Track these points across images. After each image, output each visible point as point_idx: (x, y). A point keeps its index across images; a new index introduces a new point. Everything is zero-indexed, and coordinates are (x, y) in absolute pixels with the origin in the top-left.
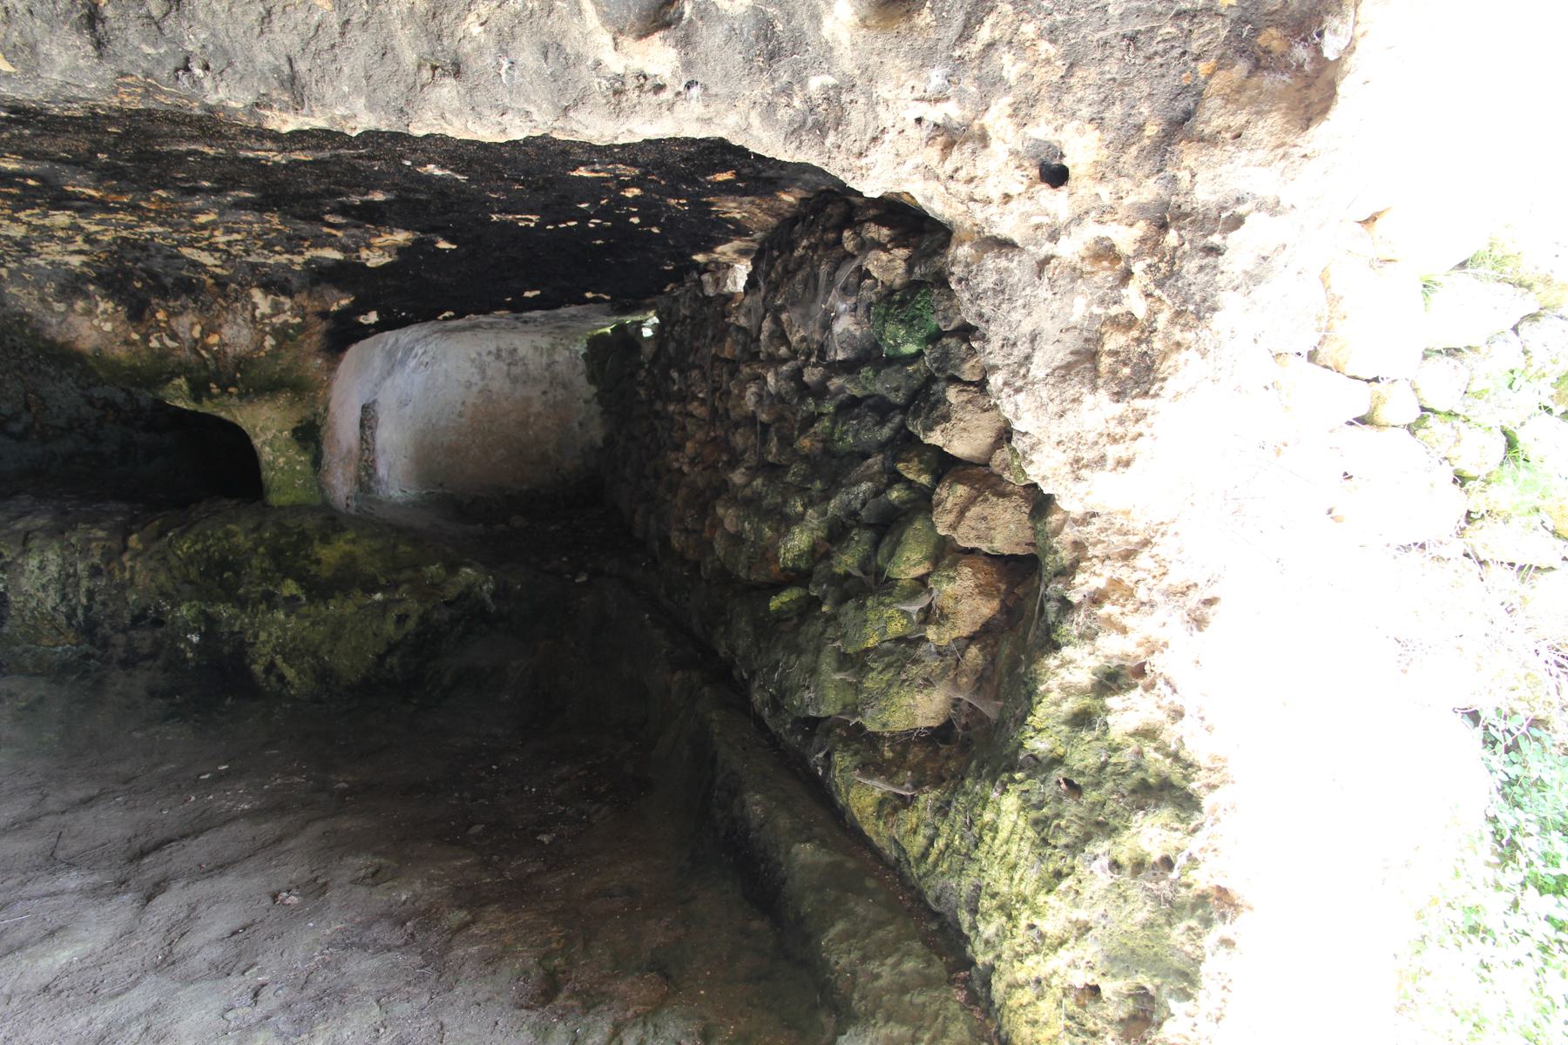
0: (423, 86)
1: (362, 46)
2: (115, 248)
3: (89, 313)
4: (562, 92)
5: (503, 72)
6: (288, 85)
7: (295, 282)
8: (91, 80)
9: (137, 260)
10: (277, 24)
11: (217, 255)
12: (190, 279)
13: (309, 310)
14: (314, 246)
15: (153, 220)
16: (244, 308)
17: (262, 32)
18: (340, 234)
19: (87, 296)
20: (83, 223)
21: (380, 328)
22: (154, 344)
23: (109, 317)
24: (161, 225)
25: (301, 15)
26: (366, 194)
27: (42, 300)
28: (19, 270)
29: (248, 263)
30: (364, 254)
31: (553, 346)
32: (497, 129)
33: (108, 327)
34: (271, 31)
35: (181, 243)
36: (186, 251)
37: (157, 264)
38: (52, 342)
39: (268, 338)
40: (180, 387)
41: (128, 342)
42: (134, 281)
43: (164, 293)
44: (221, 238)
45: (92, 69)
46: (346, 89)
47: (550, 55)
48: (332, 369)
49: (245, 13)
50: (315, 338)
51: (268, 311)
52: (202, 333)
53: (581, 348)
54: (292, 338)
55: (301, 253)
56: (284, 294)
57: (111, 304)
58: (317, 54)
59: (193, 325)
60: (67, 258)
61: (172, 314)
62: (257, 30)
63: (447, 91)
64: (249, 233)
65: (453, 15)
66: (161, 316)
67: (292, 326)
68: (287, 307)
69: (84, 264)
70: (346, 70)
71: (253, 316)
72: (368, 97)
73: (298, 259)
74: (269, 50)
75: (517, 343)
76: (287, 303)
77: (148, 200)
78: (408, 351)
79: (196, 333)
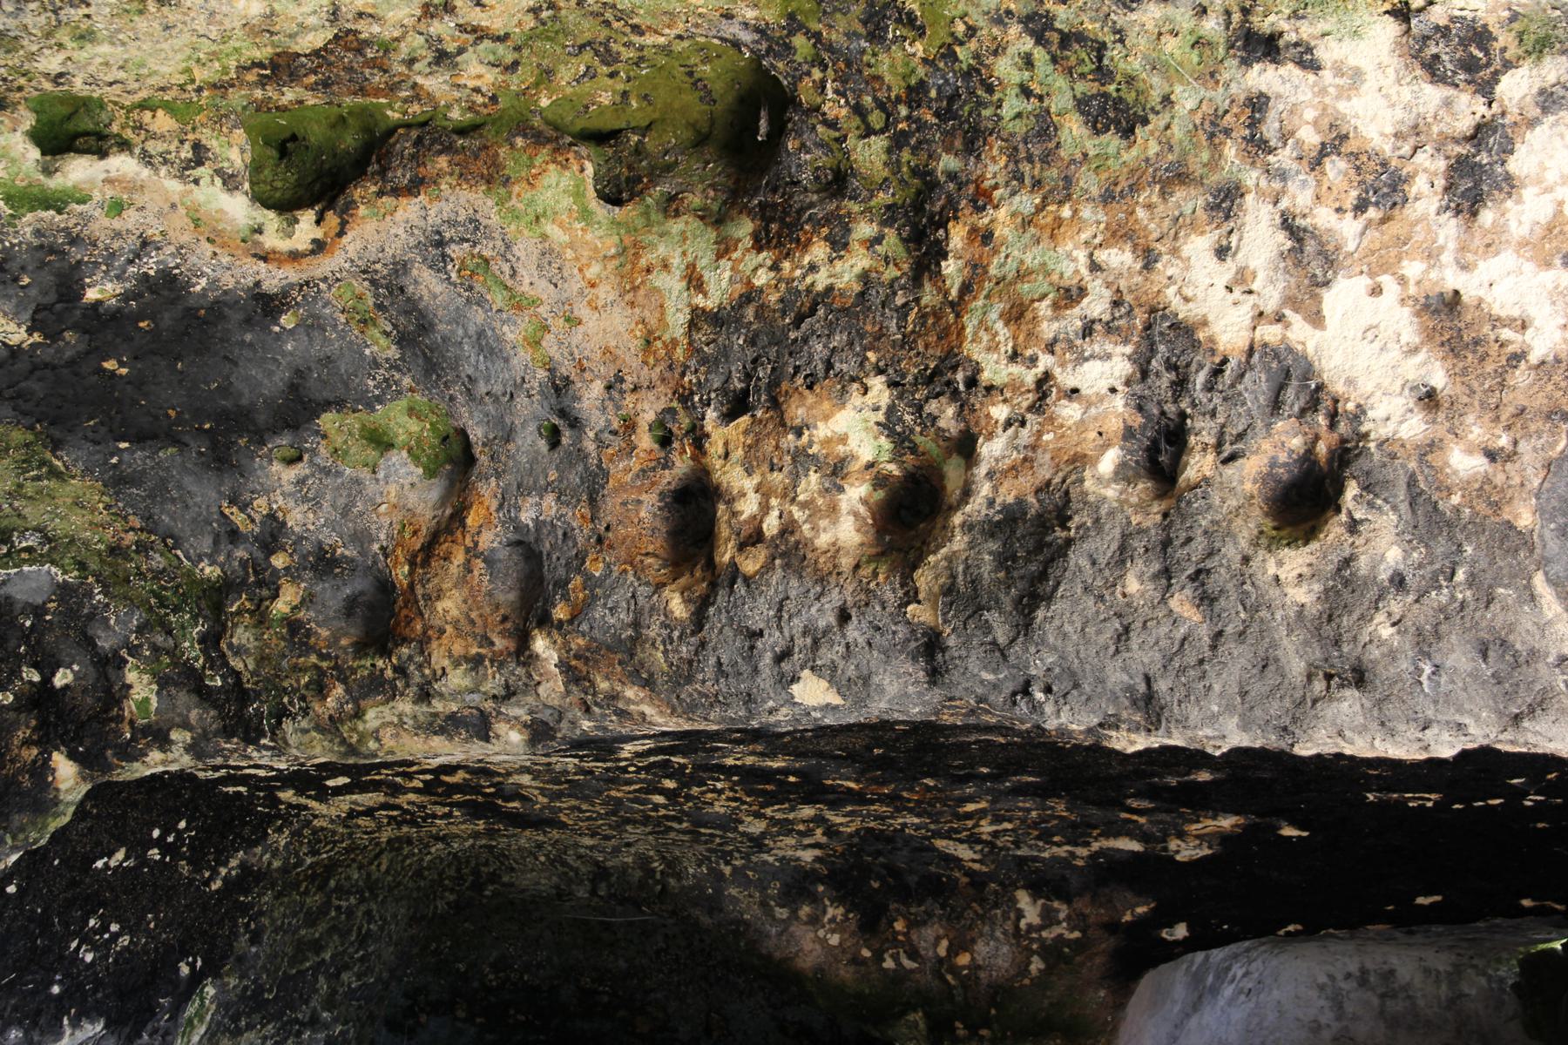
0: (1315, 702)
1: (1238, 659)
2: (856, 840)
3: (814, 921)
4: (1509, 696)
5: (1424, 678)
6: (1141, 704)
7: (1075, 882)
8: (915, 705)
9: (879, 853)
10: (1135, 642)
11: (979, 847)
12: (939, 876)
13: (1092, 919)
14: (1106, 835)
15: (911, 811)
16: (1006, 917)
17: (1117, 651)
18: (1142, 820)
19: (814, 899)
20: (831, 816)
21: (1188, 946)
22: (889, 964)
23: (837, 926)
24: (918, 815)
25: (1164, 630)
26: (1188, 774)
27: (764, 904)
28: (744, 867)
29: (1015, 857)
30: (1173, 844)
31: (1458, 970)
32: (1417, 746)
33: (834, 940)
34: (1128, 650)
35: (938, 834)
36: (940, 844)
37: (901, 860)
38: (770, 956)
39: (1035, 958)
40: (916, 1023)
41: (856, 961)
42: (872, 881)
43: (906, 895)
44: (986, 828)
45: (920, 694)
46: (1215, 708)
47: (1491, 653)
48: (1120, 1001)
49: (1099, 632)
50: (1098, 960)
51: (1036, 921)
52: (948, 950)
53: (1508, 972)
54: (1068, 960)
55: (1087, 844)
56: (1059, 898)
57: (841, 910)
58: (1183, 670)
59: (938, 939)
60: (800, 853)
61: (913, 924)
62: (1113, 648)
63: (1349, 704)
64: (1023, 821)
65: (1355, 616)
66: (899, 926)
67: (1069, 943)
68: (1062, 916)
69: (817, 859)
70: (1217, 687)
71: (1017, 927)
72: (1242, 716)
73: (1082, 852)
74: (1125, 669)
75: (1394, 961)
76: (1063, 910)
77: (911, 790)
78: (1223, 973)
79: (942, 951)
